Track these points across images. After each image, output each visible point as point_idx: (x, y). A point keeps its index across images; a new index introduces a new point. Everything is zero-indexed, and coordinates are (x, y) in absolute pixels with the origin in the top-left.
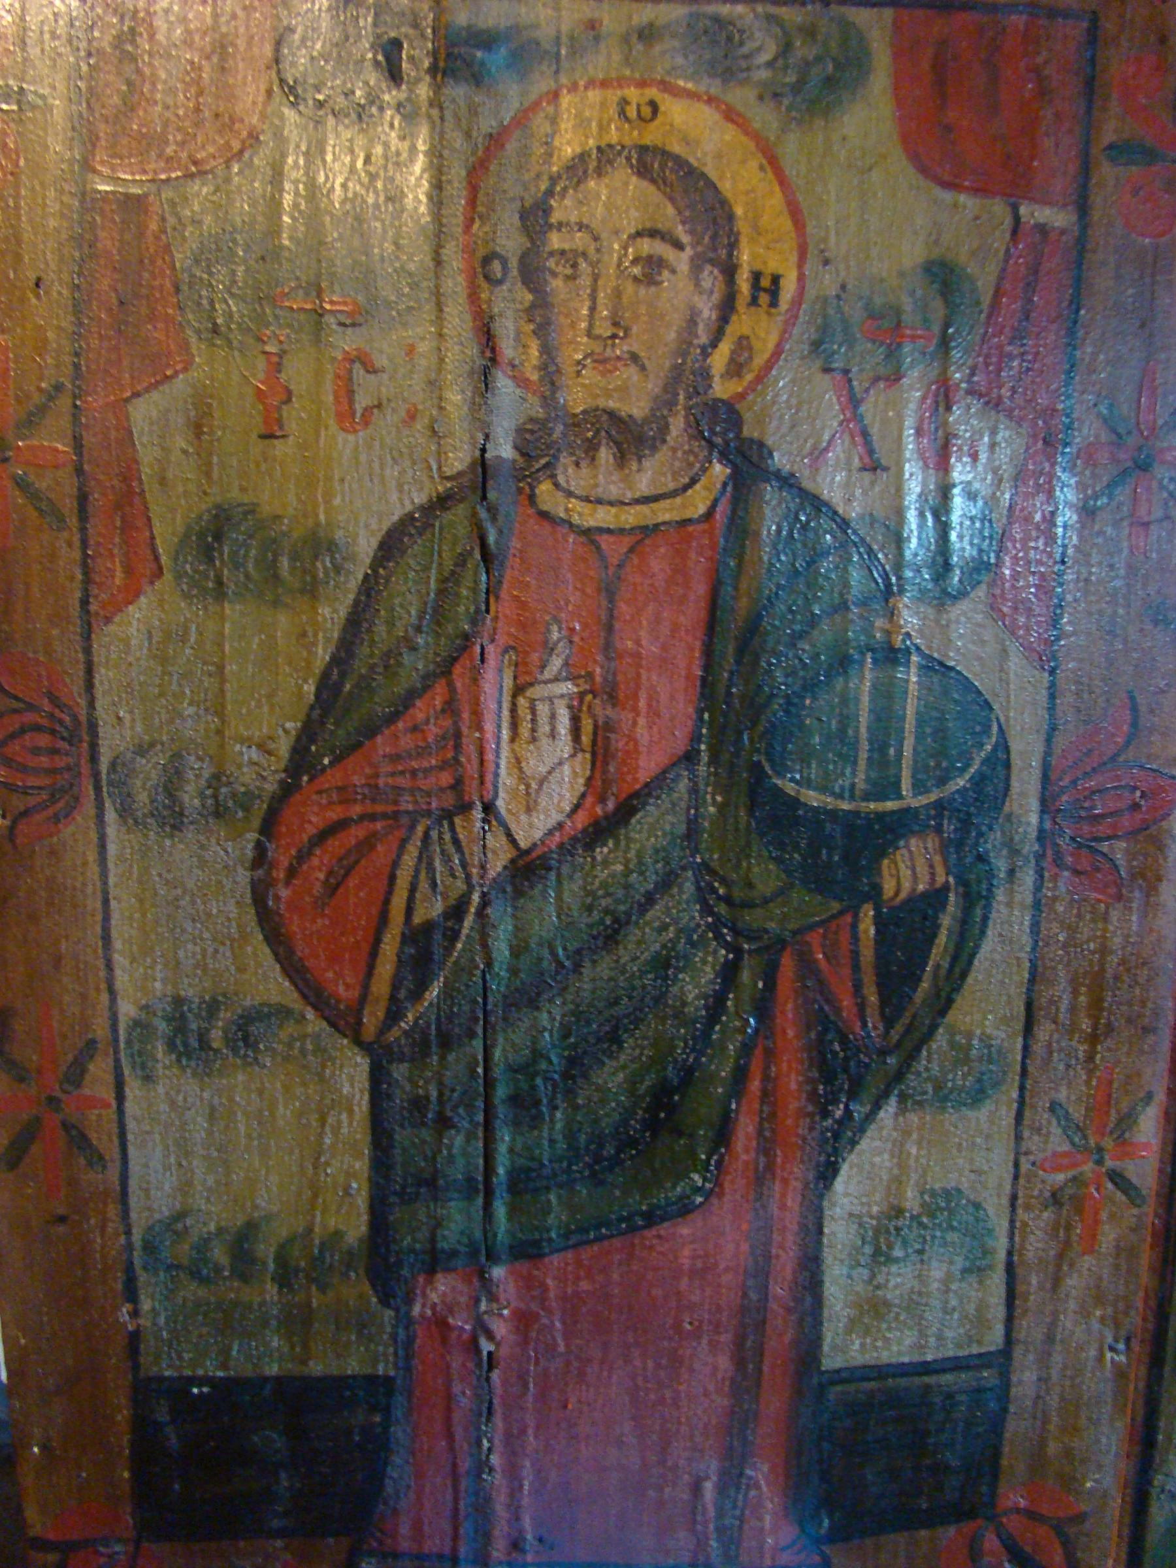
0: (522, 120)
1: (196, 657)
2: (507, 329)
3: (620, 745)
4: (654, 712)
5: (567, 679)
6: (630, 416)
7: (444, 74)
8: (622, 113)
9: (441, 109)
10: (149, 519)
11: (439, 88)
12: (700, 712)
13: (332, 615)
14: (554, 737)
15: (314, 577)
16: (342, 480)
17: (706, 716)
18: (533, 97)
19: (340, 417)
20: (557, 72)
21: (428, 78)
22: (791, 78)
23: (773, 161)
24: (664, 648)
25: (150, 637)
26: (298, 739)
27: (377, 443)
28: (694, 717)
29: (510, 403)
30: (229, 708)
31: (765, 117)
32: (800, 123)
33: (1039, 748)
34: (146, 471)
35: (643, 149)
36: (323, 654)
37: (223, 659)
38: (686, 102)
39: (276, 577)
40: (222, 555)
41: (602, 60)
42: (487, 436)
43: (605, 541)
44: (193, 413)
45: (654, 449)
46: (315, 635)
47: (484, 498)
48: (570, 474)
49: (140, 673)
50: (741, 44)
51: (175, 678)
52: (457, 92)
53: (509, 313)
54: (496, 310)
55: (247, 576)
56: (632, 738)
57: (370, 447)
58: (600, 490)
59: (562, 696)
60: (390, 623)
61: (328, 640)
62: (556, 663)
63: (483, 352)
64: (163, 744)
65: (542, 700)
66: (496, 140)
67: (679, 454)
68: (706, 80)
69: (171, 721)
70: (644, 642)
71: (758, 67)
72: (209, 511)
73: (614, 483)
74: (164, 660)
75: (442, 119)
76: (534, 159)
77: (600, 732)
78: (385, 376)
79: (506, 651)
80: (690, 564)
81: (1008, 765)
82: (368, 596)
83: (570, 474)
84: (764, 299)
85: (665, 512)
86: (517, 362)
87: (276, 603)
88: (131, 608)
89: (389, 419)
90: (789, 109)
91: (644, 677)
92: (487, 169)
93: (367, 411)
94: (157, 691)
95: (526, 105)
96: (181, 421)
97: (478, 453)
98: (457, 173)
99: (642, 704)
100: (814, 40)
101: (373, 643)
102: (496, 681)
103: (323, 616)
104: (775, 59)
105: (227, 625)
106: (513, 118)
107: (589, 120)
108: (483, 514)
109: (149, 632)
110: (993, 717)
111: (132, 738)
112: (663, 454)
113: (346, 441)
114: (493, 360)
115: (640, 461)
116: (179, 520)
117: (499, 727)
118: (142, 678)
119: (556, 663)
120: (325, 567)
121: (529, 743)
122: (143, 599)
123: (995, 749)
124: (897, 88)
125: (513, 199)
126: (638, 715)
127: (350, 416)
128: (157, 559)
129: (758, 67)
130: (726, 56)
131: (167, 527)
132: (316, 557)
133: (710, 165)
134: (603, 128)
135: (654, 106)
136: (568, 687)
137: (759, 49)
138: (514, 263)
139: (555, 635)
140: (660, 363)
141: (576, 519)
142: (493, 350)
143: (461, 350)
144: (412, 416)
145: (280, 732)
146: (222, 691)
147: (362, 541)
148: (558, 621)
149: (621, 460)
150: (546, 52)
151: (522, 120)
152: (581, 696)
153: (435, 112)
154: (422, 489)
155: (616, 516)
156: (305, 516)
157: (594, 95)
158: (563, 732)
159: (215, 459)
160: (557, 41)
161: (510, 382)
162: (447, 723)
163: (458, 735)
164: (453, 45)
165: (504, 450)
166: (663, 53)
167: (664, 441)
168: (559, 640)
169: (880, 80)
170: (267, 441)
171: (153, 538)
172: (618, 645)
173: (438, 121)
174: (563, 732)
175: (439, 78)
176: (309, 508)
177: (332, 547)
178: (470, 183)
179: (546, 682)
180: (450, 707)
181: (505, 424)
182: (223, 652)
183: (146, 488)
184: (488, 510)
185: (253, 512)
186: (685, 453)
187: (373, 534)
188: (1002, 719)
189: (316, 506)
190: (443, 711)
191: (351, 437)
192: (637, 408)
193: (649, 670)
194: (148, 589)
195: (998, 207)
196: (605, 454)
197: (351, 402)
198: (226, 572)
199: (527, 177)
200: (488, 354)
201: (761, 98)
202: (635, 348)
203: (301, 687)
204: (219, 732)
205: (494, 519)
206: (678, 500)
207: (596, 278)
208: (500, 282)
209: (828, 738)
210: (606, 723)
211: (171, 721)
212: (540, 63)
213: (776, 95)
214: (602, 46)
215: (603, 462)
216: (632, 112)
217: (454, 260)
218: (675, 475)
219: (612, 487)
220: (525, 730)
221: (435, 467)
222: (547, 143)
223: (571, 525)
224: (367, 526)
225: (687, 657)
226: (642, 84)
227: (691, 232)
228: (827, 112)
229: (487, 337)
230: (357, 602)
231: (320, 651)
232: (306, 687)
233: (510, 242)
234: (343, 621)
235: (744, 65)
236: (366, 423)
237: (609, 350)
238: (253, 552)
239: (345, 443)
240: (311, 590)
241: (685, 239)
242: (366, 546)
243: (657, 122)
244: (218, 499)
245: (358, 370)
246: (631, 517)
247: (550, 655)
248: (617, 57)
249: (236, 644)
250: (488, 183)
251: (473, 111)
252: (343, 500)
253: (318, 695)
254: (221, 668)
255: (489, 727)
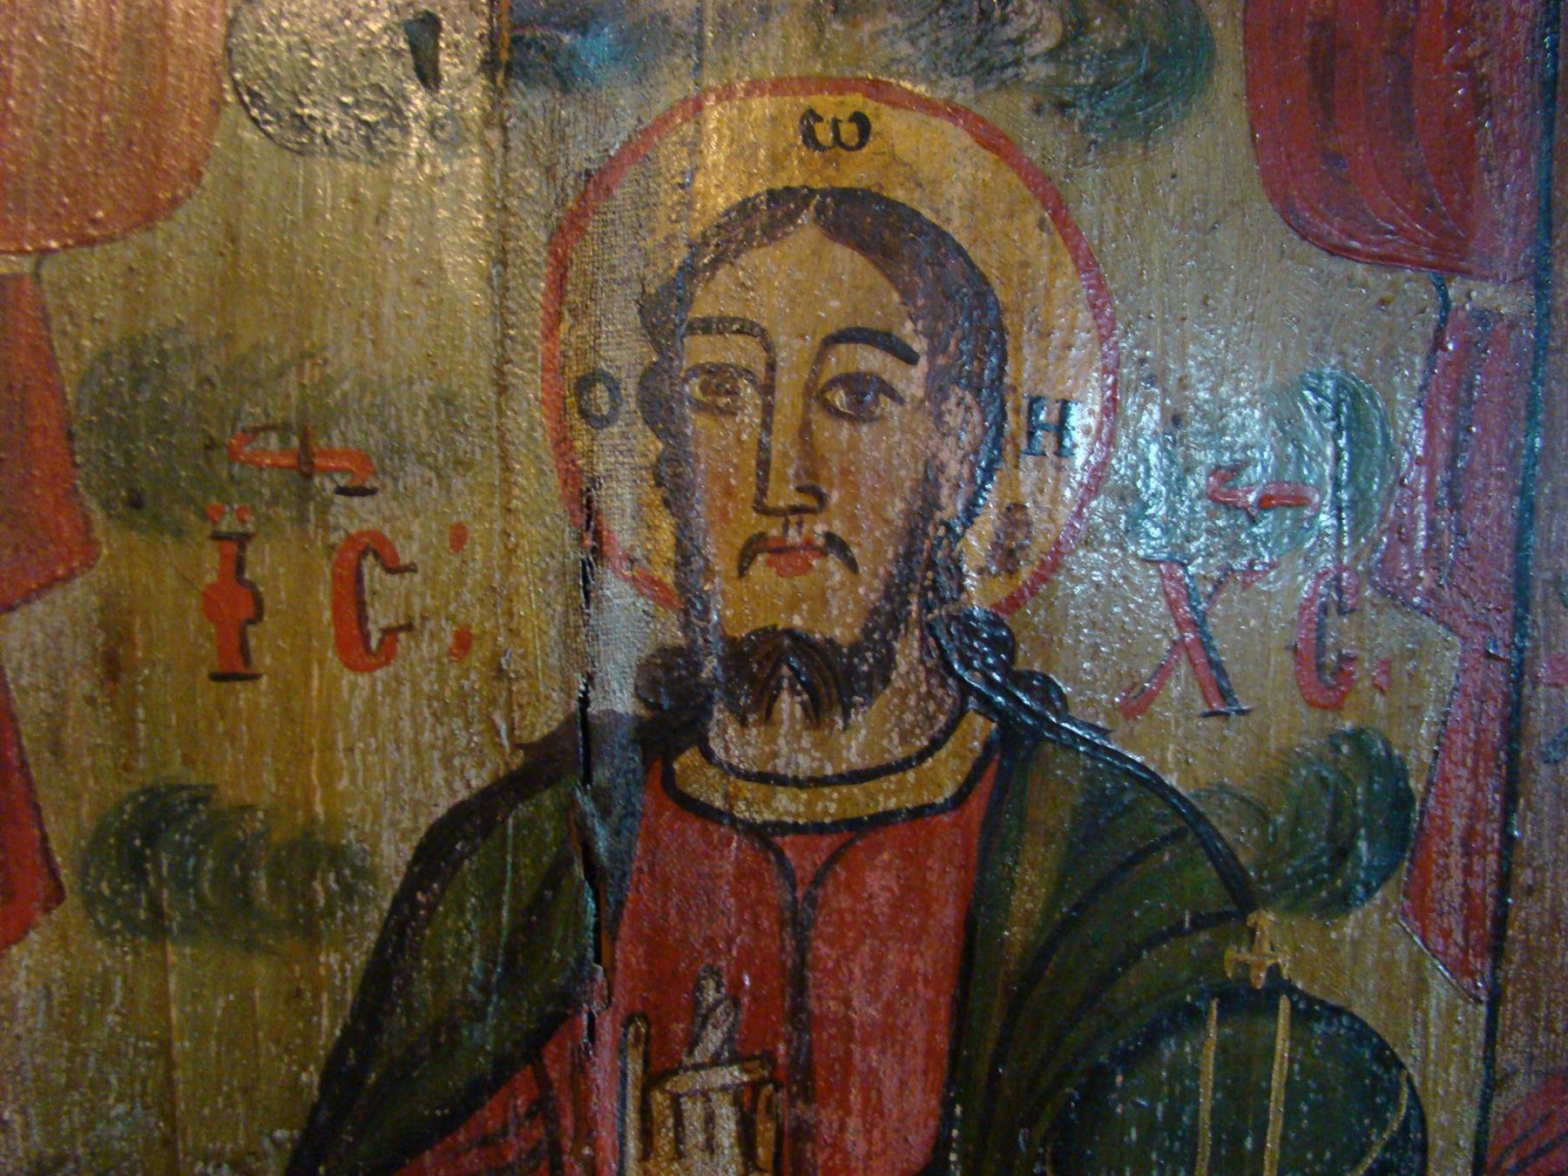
0: (638, 149)
1: (125, 1027)
2: (622, 501)
3: (821, 1159)
4: (874, 1110)
5: (731, 1062)
6: (831, 642)
7: (509, 72)
8: (810, 138)
9: (504, 129)
10: (38, 809)
11: (501, 94)
12: (947, 1105)
13: (342, 964)
14: (712, 1152)
15: (310, 902)
16: (350, 750)
17: (958, 1110)
18: (659, 108)
19: (343, 647)
20: (699, 67)
21: (482, 81)
22: (1087, 79)
23: (1060, 217)
24: (889, 1009)
25: (49, 996)
26: (296, 1156)
27: (406, 691)
28: (940, 1111)
29: (629, 627)
30: (182, 1106)
31: (1042, 140)
32: (1102, 150)
33: (1470, 1116)
34: (28, 732)
35: (846, 196)
36: (329, 1026)
37: (169, 1029)
38: (915, 117)
39: (248, 903)
40: (158, 866)
41: (774, 50)
42: (590, 678)
43: (785, 841)
44: (101, 639)
45: (870, 694)
46: (316, 997)
47: (587, 778)
48: (732, 740)
49: (33, 1053)
50: (1005, 21)
51: (92, 1059)
52: (530, 101)
53: (624, 472)
54: (601, 468)
55: (199, 898)
56: (837, 1146)
57: (396, 695)
58: (780, 763)
59: (724, 1089)
60: (438, 977)
61: (336, 1005)
62: (713, 1038)
63: (581, 539)
64: (77, 1160)
65: (692, 1095)
66: (597, 182)
67: (912, 701)
68: (949, 81)
69: (89, 1126)
70: (856, 1003)
71: (1033, 59)
72: (132, 798)
73: (805, 751)
74: (73, 1032)
75: (506, 147)
76: (661, 214)
77: (786, 1142)
78: (417, 578)
79: (629, 1020)
80: (932, 878)
81: (1423, 1148)
82: (402, 934)
83: (732, 740)
84: (1045, 440)
85: (887, 797)
86: (638, 553)
87: (250, 946)
88: (14, 950)
89: (422, 652)
90: (1084, 128)
91: (857, 1056)
92: (582, 230)
93: (390, 632)
94: (63, 1080)
95: (648, 122)
96: (82, 653)
97: (574, 705)
98: (533, 237)
99: (855, 1097)
100: (1124, 16)
101: (409, 1010)
102: (611, 1074)
103: (329, 967)
104: (1061, 46)
105: (173, 981)
106: (625, 145)
107: (756, 147)
108: (587, 805)
109: (47, 988)
110: (1403, 1080)
111: (27, 1152)
112: (886, 699)
113: (353, 687)
114: (598, 552)
115: (846, 716)
116: (86, 809)
117: (622, 1137)
118: (39, 1060)
119: (713, 1038)
120: (327, 889)
121: (672, 1160)
122: (33, 936)
123: (1405, 1126)
124: (1252, 92)
125: (626, 281)
126: (848, 1112)
127: (360, 647)
128: (54, 873)
129: (1033, 59)
130: (979, 41)
131: (68, 820)
132: (312, 876)
133: (956, 222)
134: (776, 161)
135: (862, 122)
136: (732, 1075)
137: (1035, 29)
138: (630, 387)
139: (711, 995)
140: (876, 551)
141: (741, 810)
142: (597, 535)
143: (546, 529)
144: (464, 642)
145: (267, 1143)
146: (169, 1082)
147: (387, 849)
148: (715, 973)
149: (815, 713)
150: (682, 35)
151: (638, 149)
152: (755, 1086)
153: (494, 136)
154: (482, 765)
155: (809, 804)
156: (293, 808)
157: (762, 106)
158: (726, 1143)
159: (141, 713)
160: (699, 15)
161: (626, 588)
162: (539, 1132)
163: (556, 1149)
164: (523, 24)
165: (619, 699)
166: (874, 37)
167: (887, 681)
168: (718, 1003)
169: (1228, 82)
170: (224, 685)
171: (45, 839)
172: (813, 1004)
173: (500, 152)
174: (726, 1143)
175: (500, 77)
176: (298, 794)
177: (337, 856)
178: (554, 254)
179: (697, 1067)
180: (543, 1108)
181: (620, 657)
182: (168, 1020)
183: (31, 760)
184: (595, 799)
185: (206, 799)
186: (920, 698)
187: (404, 836)
188: (1416, 1081)
189: (308, 792)
190: (530, 1115)
191: (363, 680)
192: (841, 627)
193: (864, 1043)
194: (40, 918)
195: (1414, 287)
196: (788, 706)
197: (362, 619)
198: (165, 893)
199: (649, 243)
200: (589, 542)
201: (1038, 109)
202: (838, 527)
203: (297, 1077)
204: (168, 1143)
205: (605, 812)
206: (911, 776)
207: (768, 410)
208: (607, 421)
209: (1150, 1130)
210: (798, 1128)
211: (89, 1126)
212: (670, 52)
213: (1062, 107)
214: (775, 21)
215: (785, 716)
216: (824, 134)
217: (530, 385)
218: (905, 738)
219: (801, 758)
220: (664, 1141)
221: (503, 728)
222: (682, 186)
223: (734, 821)
224: (394, 824)
225: (924, 1028)
226: (841, 86)
227: (931, 335)
228: (1146, 133)
229: (587, 512)
230: (381, 943)
231: (325, 1022)
232: (304, 1077)
233: (624, 353)
234: (360, 974)
235: (1008, 53)
236: (387, 651)
237: (792, 532)
238: (210, 863)
239: (357, 688)
240: (307, 928)
241: (919, 345)
242: (393, 856)
243: (865, 150)
244: (149, 780)
245: (372, 571)
246: (830, 805)
247: (703, 1026)
248: (799, 43)
249: (188, 1009)
250: (583, 255)
251: (558, 133)
252: (353, 781)
253: (325, 1086)
254: (166, 1046)
255: (606, 1136)
